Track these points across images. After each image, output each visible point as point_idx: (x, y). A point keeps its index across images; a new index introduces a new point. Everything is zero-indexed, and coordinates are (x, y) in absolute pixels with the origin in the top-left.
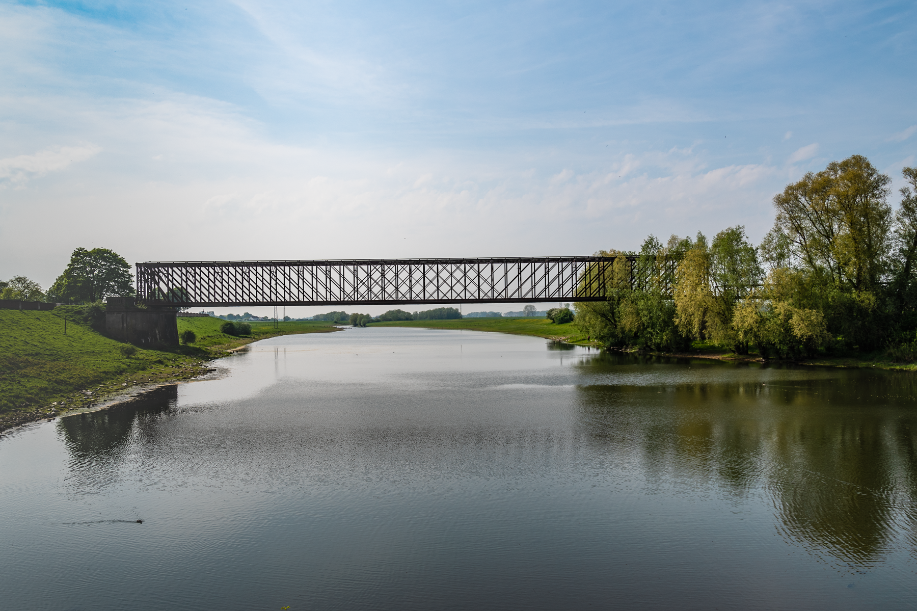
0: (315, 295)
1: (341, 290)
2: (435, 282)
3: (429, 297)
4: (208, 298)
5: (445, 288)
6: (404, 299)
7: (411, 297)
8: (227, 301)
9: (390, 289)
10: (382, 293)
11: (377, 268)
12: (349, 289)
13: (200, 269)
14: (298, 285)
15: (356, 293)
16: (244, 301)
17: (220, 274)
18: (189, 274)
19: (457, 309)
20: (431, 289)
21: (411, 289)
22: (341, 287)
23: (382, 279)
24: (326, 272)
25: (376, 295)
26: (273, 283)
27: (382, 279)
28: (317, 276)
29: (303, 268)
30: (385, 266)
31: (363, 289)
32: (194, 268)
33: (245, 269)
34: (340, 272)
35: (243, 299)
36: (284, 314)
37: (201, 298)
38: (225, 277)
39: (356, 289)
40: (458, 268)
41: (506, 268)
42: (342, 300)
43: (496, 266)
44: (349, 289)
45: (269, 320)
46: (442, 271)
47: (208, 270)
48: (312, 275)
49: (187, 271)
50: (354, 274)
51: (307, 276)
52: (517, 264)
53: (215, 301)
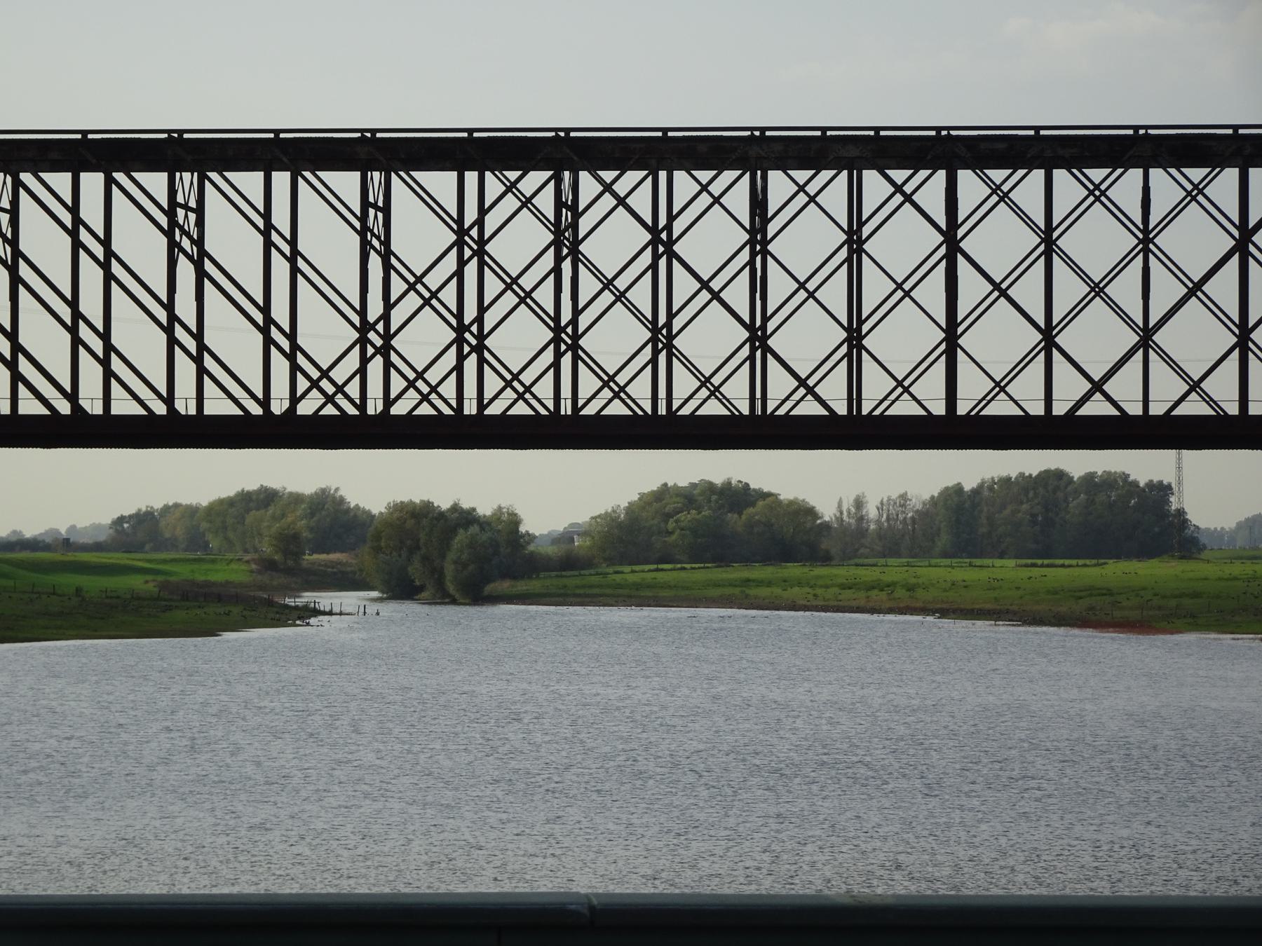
0: (91, 373)
2: (1126, 290)
3: (987, 399)
6: (810, 408)
10: (556, 365)
11: (621, 188)
15: (471, 364)
19: (1161, 491)
21: (855, 339)
23: (557, 270)
24: (171, 213)
25: (607, 380)
27: (557, 270)
29: (18, 184)
30: (584, 176)
40: (1195, 193)
42: (278, 407)
46: (1077, 214)
50: (363, 232)
52: (845, 173)
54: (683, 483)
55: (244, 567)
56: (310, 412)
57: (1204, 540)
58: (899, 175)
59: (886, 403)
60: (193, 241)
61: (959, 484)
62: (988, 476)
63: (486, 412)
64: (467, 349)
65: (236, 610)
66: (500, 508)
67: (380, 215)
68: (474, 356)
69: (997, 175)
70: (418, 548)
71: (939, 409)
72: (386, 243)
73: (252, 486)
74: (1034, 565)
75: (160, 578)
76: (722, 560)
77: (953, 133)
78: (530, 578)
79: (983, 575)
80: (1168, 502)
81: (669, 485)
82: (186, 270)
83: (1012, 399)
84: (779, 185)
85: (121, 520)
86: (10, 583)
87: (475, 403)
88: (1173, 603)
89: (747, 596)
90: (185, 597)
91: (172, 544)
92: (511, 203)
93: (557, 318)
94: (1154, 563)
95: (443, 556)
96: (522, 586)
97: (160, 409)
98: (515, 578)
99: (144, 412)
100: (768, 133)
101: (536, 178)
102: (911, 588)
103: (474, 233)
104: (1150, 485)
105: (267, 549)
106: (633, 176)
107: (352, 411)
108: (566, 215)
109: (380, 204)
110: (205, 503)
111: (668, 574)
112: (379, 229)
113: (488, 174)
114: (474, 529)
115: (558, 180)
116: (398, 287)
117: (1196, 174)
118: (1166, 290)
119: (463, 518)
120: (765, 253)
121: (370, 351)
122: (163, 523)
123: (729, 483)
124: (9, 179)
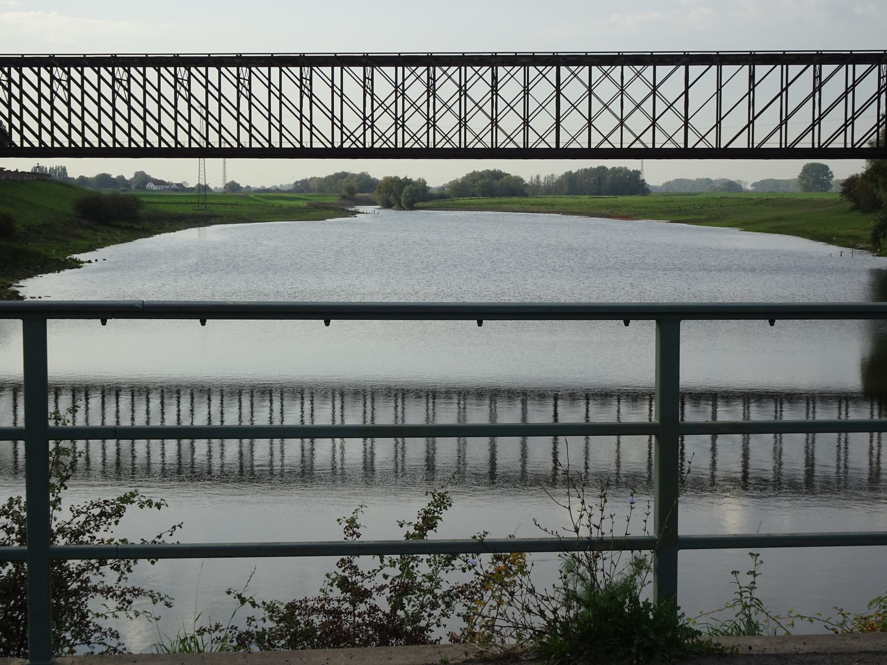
1: (333, 123)
2: (615, 107)
3: (569, 143)
4: (39, 137)
5: (605, 123)
7: (526, 141)
8: (80, 145)
9: (447, 122)
12: (352, 121)
13: (20, 71)
14: (238, 109)
16: (148, 146)
17: (64, 83)
18: (57, 84)
19: (637, 173)
20: (573, 123)
21: (526, 122)
22: (333, 116)
24: (301, 81)
25: (445, 136)
26: (244, 109)
27: (428, 100)
28: (280, 91)
29: (251, 71)
31: (384, 123)
32: (66, 69)
33: (120, 72)
34: (332, 81)
35: (146, 141)
36: (225, 176)
37: (23, 138)
38: (76, 91)
39: (368, 122)
40: (638, 74)
41: (784, 75)
42: (337, 145)
43: (761, 70)
44: (352, 121)
45: (192, 189)
46: (600, 81)
47: (38, 74)
48: (269, 87)
49: (53, 78)
50: (364, 87)
51: (321, 90)
52: (812, 66)
53: (83, 144)
54: (480, 170)
55: (336, 198)
56: (347, 147)
57: (651, 189)
58: (541, 68)
59: (536, 144)
60: (308, 90)
61: (65, 167)
62: (580, 168)
63: (426, 67)
64: (398, 126)
65: (331, 212)
66: (420, 179)
67: (370, 82)
68: (401, 128)
69: (573, 68)
70: (393, 191)
71: (554, 146)
72: (372, 91)
73: (339, 171)
74: (594, 198)
75: (309, 202)
76: (492, 195)
77: (756, 53)
78: (429, 201)
79: (578, 200)
80: (639, 177)
81: (573, 172)
82: (306, 100)
83: (609, 142)
84: (501, 71)
85: (297, 182)
86: (258, 203)
87: (401, 144)
88: (638, 210)
89: (500, 208)
90: (316, 208)
91: (313, 190)
92: (413, 78)
93: (428, 115)
94: (634, 196)
95: (401, 195)
96: (427, 204)
97: (298, 145)
98: (424, 201)
99: (549, 147)
100: (498, 54)
101: (421, 69)
102: (553, 205)
103: (463, 88)
104: (633, 171)
105: (344, 192)
106: (453, 69)
107: (361, 146)
108: (431, 81)
109: (370, 78)
110: (324, 177)
111: (474, 200)
112: (370, 86)
113: (405, 68)
114: (411, 185)
115: (428, 70)
116: (376, 105)
117: (639, 68)
118: (629, 106)
119: (408, 182)
120: (497, 94)
121: (367, 127)
122: (310, 183)
123: (495, 171)
124: (248, 70)
